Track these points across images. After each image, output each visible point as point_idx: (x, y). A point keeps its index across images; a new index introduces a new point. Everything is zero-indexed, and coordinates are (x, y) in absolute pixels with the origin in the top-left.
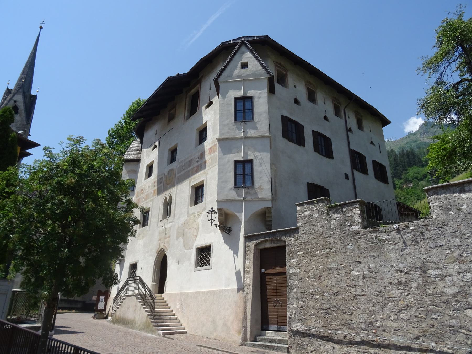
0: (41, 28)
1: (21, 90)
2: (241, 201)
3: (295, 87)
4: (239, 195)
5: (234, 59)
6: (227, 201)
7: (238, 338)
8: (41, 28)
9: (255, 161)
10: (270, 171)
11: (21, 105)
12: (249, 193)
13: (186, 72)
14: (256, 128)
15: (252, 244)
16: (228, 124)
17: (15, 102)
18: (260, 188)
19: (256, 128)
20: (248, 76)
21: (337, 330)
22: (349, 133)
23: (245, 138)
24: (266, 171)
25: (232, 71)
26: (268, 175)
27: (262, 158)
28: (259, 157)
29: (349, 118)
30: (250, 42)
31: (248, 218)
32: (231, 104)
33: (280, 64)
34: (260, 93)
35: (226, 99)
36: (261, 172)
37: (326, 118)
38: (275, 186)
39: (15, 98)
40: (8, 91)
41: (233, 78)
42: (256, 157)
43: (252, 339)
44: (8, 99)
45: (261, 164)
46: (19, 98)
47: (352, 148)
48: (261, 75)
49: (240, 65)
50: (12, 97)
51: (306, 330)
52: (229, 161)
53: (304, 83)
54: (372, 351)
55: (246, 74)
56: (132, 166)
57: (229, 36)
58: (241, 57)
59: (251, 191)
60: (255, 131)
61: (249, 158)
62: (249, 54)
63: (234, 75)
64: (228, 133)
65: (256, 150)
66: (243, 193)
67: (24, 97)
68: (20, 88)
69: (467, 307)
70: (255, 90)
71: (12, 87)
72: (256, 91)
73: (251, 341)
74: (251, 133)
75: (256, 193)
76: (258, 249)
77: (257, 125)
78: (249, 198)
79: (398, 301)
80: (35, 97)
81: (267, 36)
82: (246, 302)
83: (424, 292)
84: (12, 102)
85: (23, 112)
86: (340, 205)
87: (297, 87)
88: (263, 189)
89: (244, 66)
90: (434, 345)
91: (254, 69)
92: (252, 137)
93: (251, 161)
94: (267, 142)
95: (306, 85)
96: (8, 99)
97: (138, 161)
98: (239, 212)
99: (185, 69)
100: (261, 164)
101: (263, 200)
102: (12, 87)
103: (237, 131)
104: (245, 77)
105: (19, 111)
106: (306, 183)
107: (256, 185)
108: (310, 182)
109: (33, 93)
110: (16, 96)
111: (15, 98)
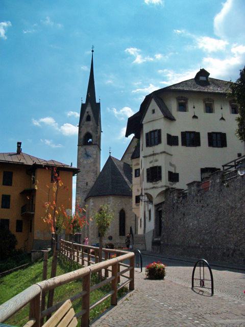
11: (91, 114)
17: (88, 112)
37: (222, 119)
80: (99, 104)
89: (154, 111)
102: (84, 102)
109: (97, 101)
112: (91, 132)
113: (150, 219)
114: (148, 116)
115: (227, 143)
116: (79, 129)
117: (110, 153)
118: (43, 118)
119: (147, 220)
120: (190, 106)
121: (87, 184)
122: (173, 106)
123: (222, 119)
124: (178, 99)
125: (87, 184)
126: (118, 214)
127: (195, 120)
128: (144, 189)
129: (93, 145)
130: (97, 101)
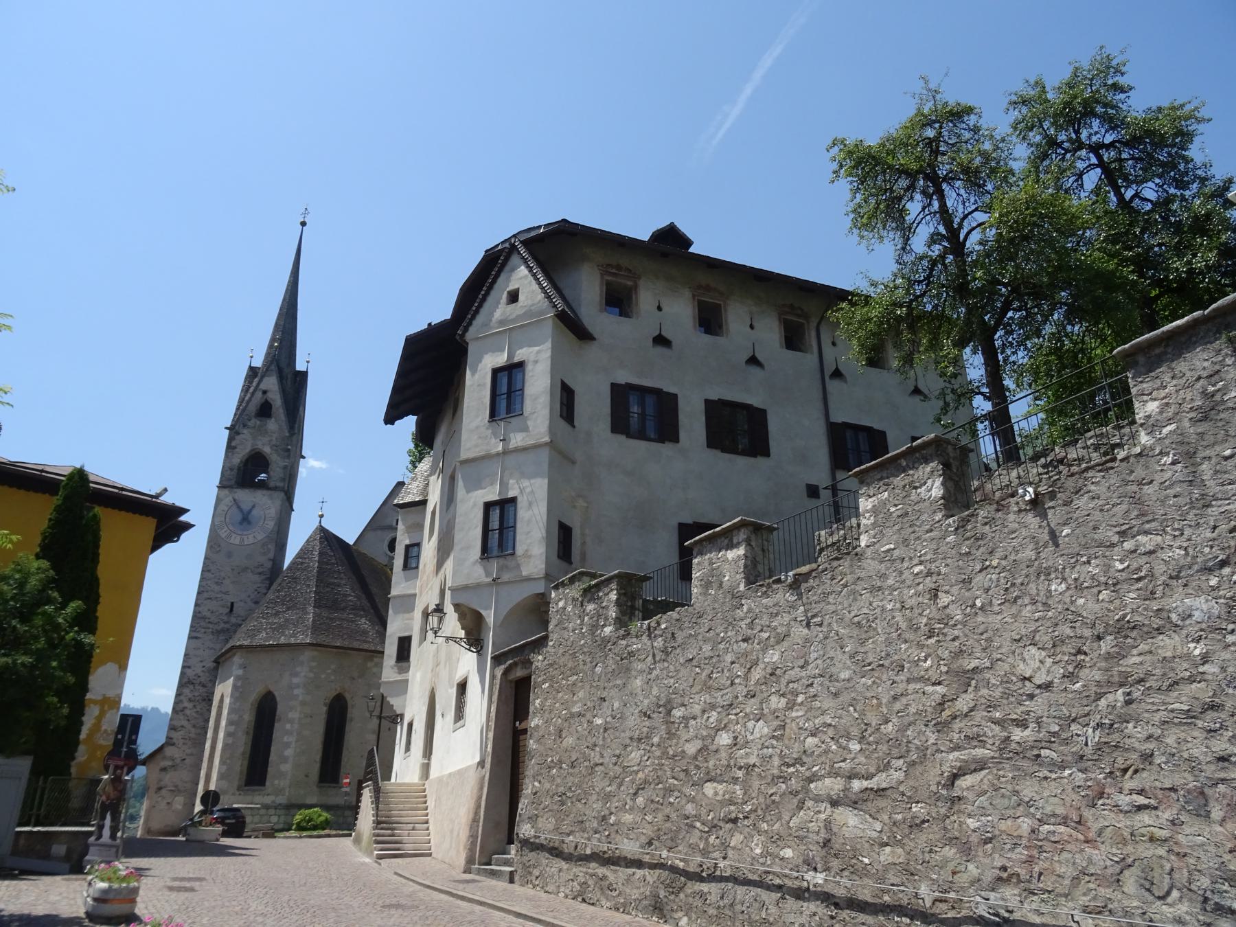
0: (303, 224)
1: (273, 367)
2: (489, 585)
3: (659, 308)
4: (488, 574)
5: (496, 286)
6: (466, 588)
7: (461, 861)
8: (303, 224)
9: (519, 499)
10: (545, 517)
11: (276, 399)
12: (507, 567)
13: (449, 317)
14: (525, 429)
15: (499, 672)
16: (477, 427)
17: (265, 392)
18: (527, 555)
19: (525, 429)
20: (519, 318)
21: (568, 835)
22: (833, 386)
23: (505, 452)
24: (538, 518)
25: (491, 314)
26: (541, 525)
27: (532, 492)
28: (528, 490)
29: (834, 344)
30: (525, 243)
31: (502, 618)
32: (484, 385)
33: (619, 267)
34: (538, 352)
35: (477, 376)
36: (529, 521)
37: (753, 361)
38: (584, 543)
39: (263, 386)
40: (253, 372)
41: (491, 328)
42: (521, 491)
43: (484, 860)
44: (251, 390)
45: (530, 504)
46: (271, 382)
47: (838, 417)
48: (542, 313)
49: (505, 295)
50: (258, 384)
51: (536, 837)
52: (475, 505)
53: (687, 294)
54: (862, 917)
55: (513, 316)
56: (412, 515)
57: (495, 237)
58: (508, 279)
59: (510, 562)
60: (524, 434)
61: (511, 494)
62: (523, 270)
63: (494, 320)
64: (476, 446)
65: (524, 475)
66: (494, 565)
67: (281, 378)
68: (272, 362)
69: (707, 778)
70: (530, 346)
71: (258, 362)
72: (531, 349)
73: (480, 864)
74: (517, 440)
75: (518, 566)
76: (511, 681)
77: (529, 423)
78: (506, 577)
79: (637, 772)
80: (304, 375)
81: (564, 221)
82: (481, 788)
83: (665, 753)
84: (259, 395)
85: (281, 411)
86: (595, 585)
87: (665, 308)
88: (530, 557)
89: (514, 297)
90: (665, 854)
91: (530, 302)
92: (517, 450)
93: (513, 500)
94: (544, 455)
95: (694, 296)
96: (251, 390)
97: (423, 503)
98: (486, 609)
99: (443, 311)
100: (530, 504)
101: (529, 579)
102: (258, 362)
103: (493, 440)
104: (513, 321)
105: (274, 410)
106: (674, 523)
107: (520, 550)
108: (690, 521)
109: (300, 366)
110: (266, 380)
111: (263, 386)
112: (267, 450)
113: (460, 714)
114: (497, 311)
115: (772, 443)
116: (230, 439)
117: (321, 516)
118: (79, 732)
119: (443, 724)
120: (646, 298)
121: (231, 610)
122: (588, 288)
123: (753, 361)
124: (605, 270)
125: (231, 610)
126: (325, 709)
127: (660, 350)
128: (452, 590)
129: (269, 489)
130: (300, 366)
